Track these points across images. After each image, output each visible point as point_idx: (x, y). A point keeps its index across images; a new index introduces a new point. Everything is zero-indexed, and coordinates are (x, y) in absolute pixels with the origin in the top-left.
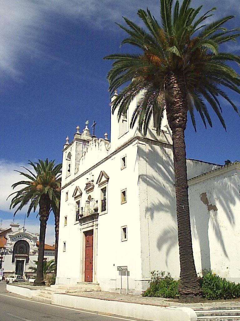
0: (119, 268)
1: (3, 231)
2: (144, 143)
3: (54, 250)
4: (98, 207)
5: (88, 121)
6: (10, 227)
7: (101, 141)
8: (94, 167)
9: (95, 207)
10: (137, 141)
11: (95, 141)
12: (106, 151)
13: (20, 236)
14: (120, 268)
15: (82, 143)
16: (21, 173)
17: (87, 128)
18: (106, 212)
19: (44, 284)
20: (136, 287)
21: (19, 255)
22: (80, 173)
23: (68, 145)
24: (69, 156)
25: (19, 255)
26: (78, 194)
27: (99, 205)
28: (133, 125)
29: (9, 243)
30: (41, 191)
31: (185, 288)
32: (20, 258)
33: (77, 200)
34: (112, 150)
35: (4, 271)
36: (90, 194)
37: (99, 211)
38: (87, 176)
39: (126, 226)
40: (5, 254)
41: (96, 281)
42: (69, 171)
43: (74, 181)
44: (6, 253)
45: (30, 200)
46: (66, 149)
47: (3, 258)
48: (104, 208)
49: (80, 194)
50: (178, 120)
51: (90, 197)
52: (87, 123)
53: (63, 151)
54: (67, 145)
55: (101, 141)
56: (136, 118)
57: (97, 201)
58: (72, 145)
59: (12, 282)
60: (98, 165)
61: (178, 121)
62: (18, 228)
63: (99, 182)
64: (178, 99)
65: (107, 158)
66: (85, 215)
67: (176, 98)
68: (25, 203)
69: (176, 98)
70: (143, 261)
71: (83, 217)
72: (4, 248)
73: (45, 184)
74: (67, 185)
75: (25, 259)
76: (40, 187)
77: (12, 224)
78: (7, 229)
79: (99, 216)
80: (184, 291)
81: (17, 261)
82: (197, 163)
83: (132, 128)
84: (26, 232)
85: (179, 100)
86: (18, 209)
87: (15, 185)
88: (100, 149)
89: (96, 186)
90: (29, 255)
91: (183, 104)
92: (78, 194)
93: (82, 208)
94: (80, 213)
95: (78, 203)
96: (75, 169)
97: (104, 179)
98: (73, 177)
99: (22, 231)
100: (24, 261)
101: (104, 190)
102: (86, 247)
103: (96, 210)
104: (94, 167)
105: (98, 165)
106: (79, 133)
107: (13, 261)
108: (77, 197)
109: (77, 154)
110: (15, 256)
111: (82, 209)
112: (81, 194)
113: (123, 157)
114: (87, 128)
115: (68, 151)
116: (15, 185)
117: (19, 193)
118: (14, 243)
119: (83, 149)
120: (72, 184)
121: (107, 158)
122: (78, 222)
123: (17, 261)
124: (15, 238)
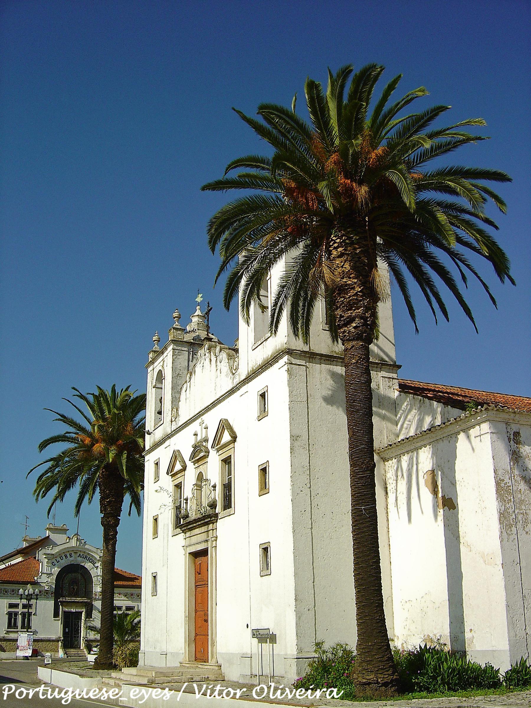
0: (254, 631)
1: (33, 543)
2: (303, 362)
3: (115, 600)
4: (217, 498)
5: (200, 295)
6: (48, 533)
7: (220, 351)
8: (208, 409)
9: (210, 499)
10: (286, 358)
11: (209, 349)
12: (231, 374)
13: (69, 556)
14: (258, 633)
15: (186, 349)
16: (60, 417)
17: (198, 312)
18: (231, 510)
19: (115, 667)
20: (286, 672)
21: (68, 599)
22: (182, 420)
23: (157, 351)
24: (160, 377)
25: (68, 599)
26: (178, 467)
27: (218, 495)
28: (277, 327)
29: (45, 572)
30: (103, 456)
31: (364, 672)
32: (71, 607)
33: (177, 482)
34: (243, 373)
35: (36, 637)
36: (201, 469)
37: (218, 509)
38: (195, 426)
39: (267, 544)
40: (37, 599)
41: (214, 660)
42: (160, 413)
43: (169, 437)
44: (37, 595)
45: (79, 478)
46: (152, 362)
47: (34, 607)
48: (228, 503)
49: (180, 468)
50: (354, 325)
51: (200, 477)
52: (199, 299)
53: (147, 367)
54: (155, 352)
55: (220, 351)
56: (281, 310)
57: (214, 487)
58: (165, 354)
59: (50, 662)
60: (214, 404)
61: (355, 328)
62: (64, 537)
63: (171, 472)
64: (353, 280)
65: (231, 392)
66: (193, 516)
67: (350, 278)
68: (68, 484)
69: (350, 278)
70: (300, 618)
71: (188, 520)
72: (35, 584)
73: (110, 440)
74: (156, 445)
75: (84, 610)
76: (98, 447)
77: (51, 526)
78: (40, 539)
79: (218, 520)
80: (360, 679)
81: (65, 613)
82: (422, 401)
83: (275, 333)
84: (86, 547)
85: (356, 281)
86: (55, 500)
87: (43, 445)
88: (219, 368)
89: (213, 453)
90: (91, 598)
91: (364, 291)
92: (178, 467)
93: (187, 500)
94: (183, 512)
95: (179, 486)
96: (171, 410)
97: (226, 437)
98: (167, 428)
99: (73, 543)
100: (81, 613)
101: (227, 461)
102: (196, 586)
103: (213, 505)
104: (208, 409)
105: (214, 404)
106: (180, 327)
107: (56, 615)
108: (176, 474)
109: (176, 376)
110: (60, 601)
111: (187, 503)
112: (184, 469)
113: (260, 393)
114: (198, 312)
115: (157, 366)
116: (43, 445)
117: (57, 460)
118: (56, 570)
119: (190, 363)
120: (167, 443)
121: (231, 392)
122: (178, 530)
123: (65, 613)
124: (58, 559)
